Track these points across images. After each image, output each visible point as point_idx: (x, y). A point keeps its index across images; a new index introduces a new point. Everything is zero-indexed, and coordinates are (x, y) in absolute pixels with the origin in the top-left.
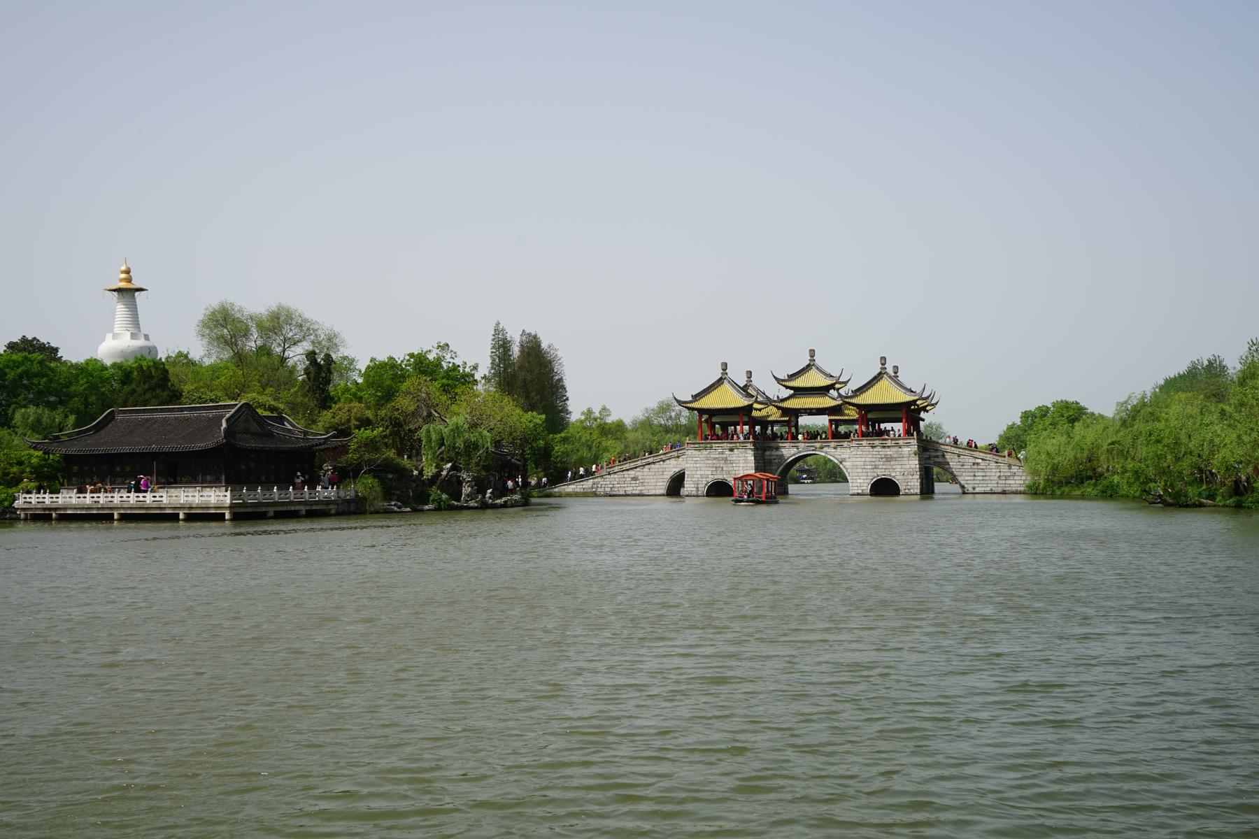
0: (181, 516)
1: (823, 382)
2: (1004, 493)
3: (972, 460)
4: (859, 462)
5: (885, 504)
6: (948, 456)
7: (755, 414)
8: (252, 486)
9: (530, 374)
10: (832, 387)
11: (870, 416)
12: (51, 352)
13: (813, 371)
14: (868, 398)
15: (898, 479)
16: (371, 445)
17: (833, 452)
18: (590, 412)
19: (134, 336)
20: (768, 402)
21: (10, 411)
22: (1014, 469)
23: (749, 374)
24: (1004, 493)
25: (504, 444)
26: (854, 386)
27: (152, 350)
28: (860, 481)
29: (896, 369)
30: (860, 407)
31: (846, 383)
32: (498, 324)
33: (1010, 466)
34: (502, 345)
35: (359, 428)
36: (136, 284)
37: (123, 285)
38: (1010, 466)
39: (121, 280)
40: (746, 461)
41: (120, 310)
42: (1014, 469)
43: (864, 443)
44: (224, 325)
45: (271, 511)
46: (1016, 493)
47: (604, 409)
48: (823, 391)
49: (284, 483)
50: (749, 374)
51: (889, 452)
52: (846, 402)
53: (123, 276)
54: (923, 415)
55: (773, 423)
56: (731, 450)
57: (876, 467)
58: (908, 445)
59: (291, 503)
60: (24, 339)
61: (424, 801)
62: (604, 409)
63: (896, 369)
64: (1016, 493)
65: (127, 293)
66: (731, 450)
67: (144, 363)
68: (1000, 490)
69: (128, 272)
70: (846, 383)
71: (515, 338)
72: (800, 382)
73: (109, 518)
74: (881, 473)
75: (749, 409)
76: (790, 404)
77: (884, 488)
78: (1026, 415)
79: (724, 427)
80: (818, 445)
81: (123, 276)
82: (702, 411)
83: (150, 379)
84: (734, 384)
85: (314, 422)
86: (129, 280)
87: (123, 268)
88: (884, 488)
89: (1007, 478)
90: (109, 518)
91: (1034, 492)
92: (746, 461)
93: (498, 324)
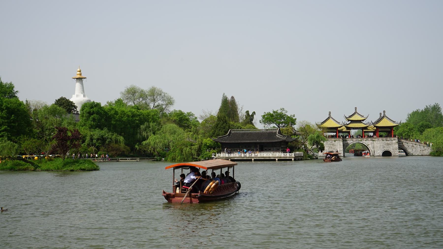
0: (253, 160)
1: (360, 118)
2: (422, 155)
3: (412, 145)
4: (378, 145)
5: (387, 160)
6: (404, 143)
12: (98, 105)
13: (356, 115)
15: (391, 151)
17: (367, 142)
19: (84, 96)
22: (425, 148)
24: (422, 155)
27: (90, 101)
28: (379, 152)
32: (224, 94)
33: (424, 147)
36: (83, 76)
37: (78, 76)
38: (424, 147)
39: (77, 74)
40: (340, 145)
41: (78, 85)
42: (425, 148)
43: (380, 139)
46: (426, 155)
48: (359, 121)
51: (388, 142)
53: (79, 73)
56: (335, 141)
57: (384, 147)
64: (426, 155)
65: (80, 79)
66: (335, 141)
68: (421, 154)
69: (80, 71)
71: (229, 98)
72: (352, 119)
73: (251, 160)
74: (386, 149)
76: (350, 126)
77: (387, 154)
80: (360, 140)
81: (79, 73)
86: (81, 74)
87: (79, 70)
88: (387, 154)
89: (423, 151)
90: (251, 160)
91: (431, 155)
92: (340, 145)
93: (224, 94)
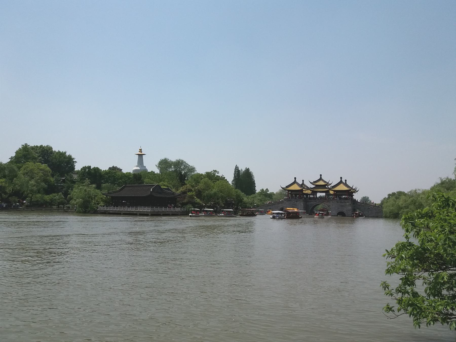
7: (304, 192)
8: (157, 206)
9: (245, 179)
10: (325, 185)
11: (337, 194)
14: (337, 188)
15: (345, 212)
16: (191, 197)
18: (263, 189)
20: (308, 188)
21: (309, 192)
23: (303, 181)
25: (235, 198)
26: (332, 185)
29: (346, 181)
30: (334, 191)
31: (331, 184)
34: (237, 171)
35: (189, 192)
44: (164, 164)
45: (138, 213)
47: (267, 189)
49: (166, 206)
50: (303, 181)
51: (342, 204)
52: (330, 189)
54: (354, 194)
55: (310, 195)
56: (297, 201)
57: (339, 208)
58: (348, 202)
59: (167, 212)
60: (113, 167)
61: (21, 301)
62: (267, 189)
63: (346, 181)
67: (217, 174)
70: (331, 184)
75: (302, 191)
78: (389, 195)
79: (296, 195)
82: (289, 191)
83: (139, 177)
84: (298, 184)
85: (178, 190)
86: (141, 152)
